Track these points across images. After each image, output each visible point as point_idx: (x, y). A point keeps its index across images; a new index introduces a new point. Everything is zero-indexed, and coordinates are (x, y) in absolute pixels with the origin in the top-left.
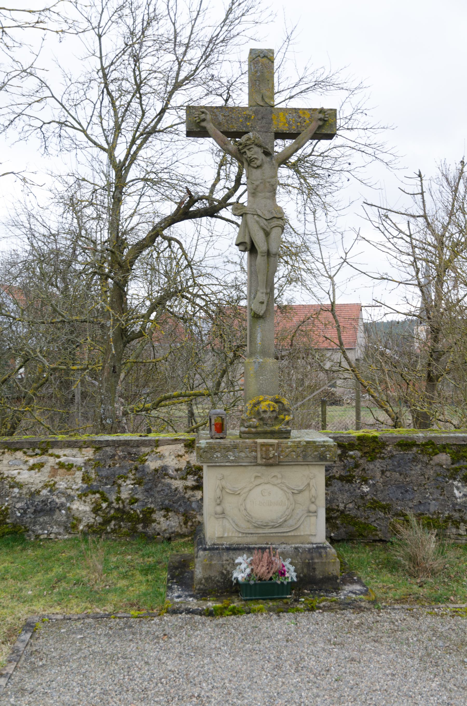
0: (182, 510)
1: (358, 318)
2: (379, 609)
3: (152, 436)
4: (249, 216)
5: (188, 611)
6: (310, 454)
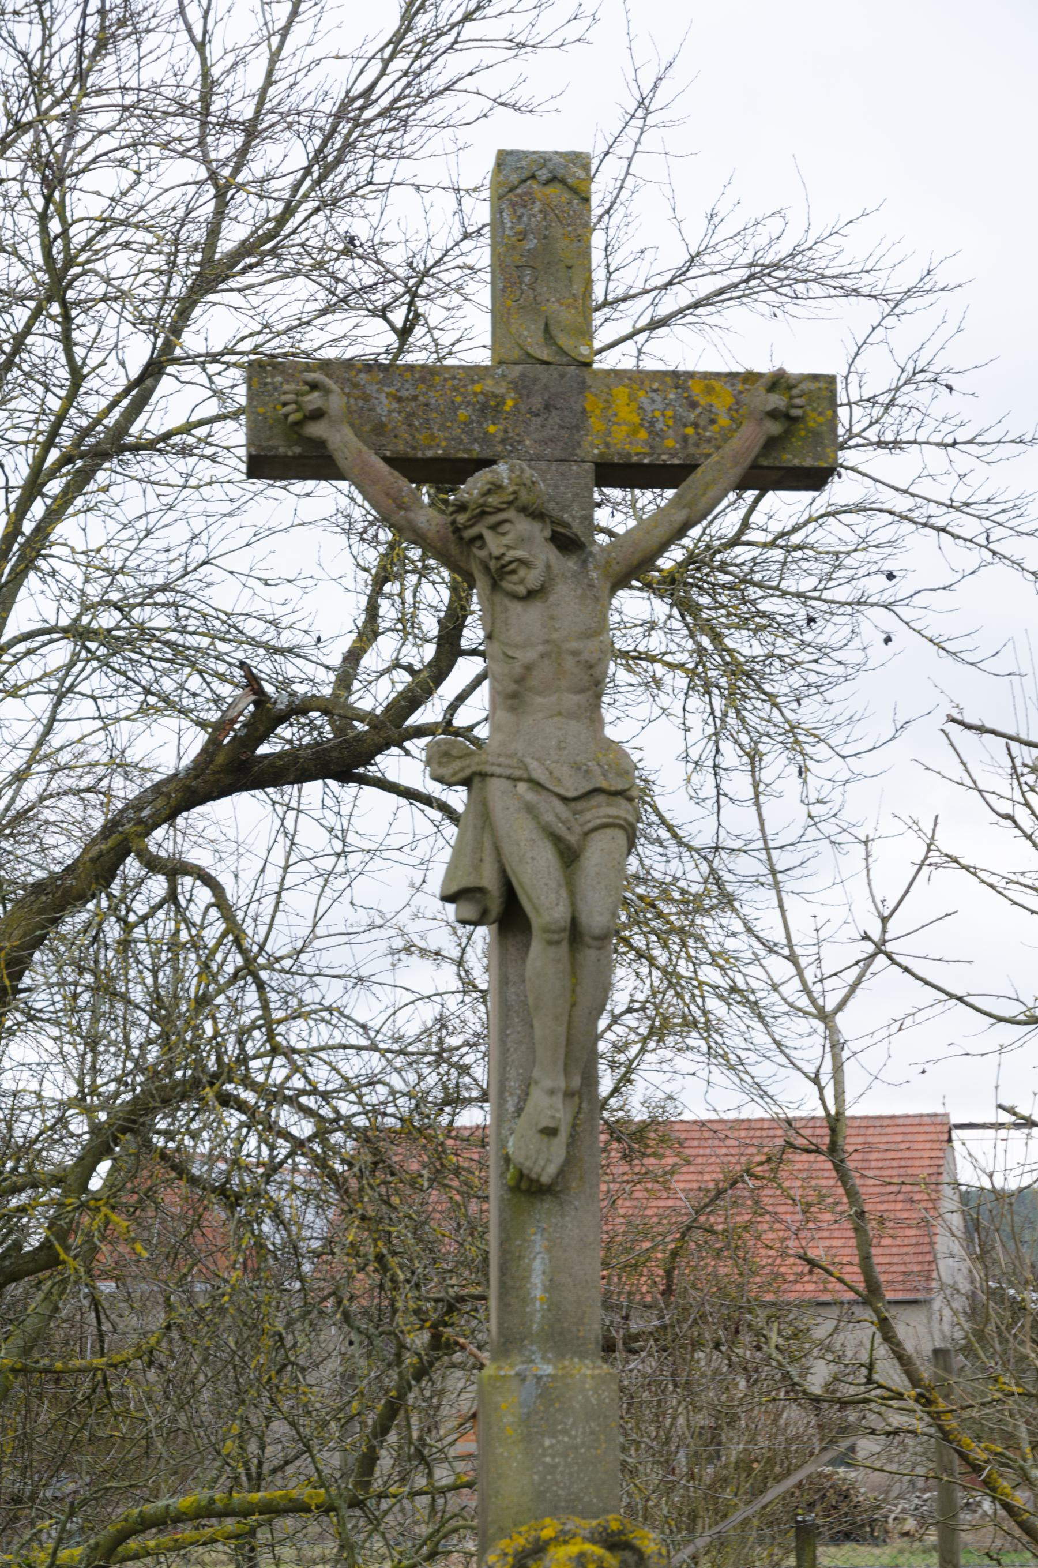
1: (938, 1175)
4: (496, 787)
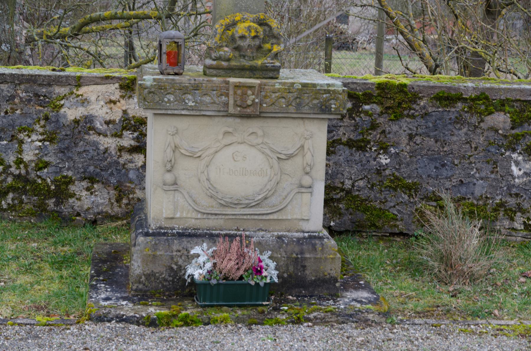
0: (113, 180)
2: (393, 323)
3: (72, 71)
5: (121, 319)
6: (307, 103)
